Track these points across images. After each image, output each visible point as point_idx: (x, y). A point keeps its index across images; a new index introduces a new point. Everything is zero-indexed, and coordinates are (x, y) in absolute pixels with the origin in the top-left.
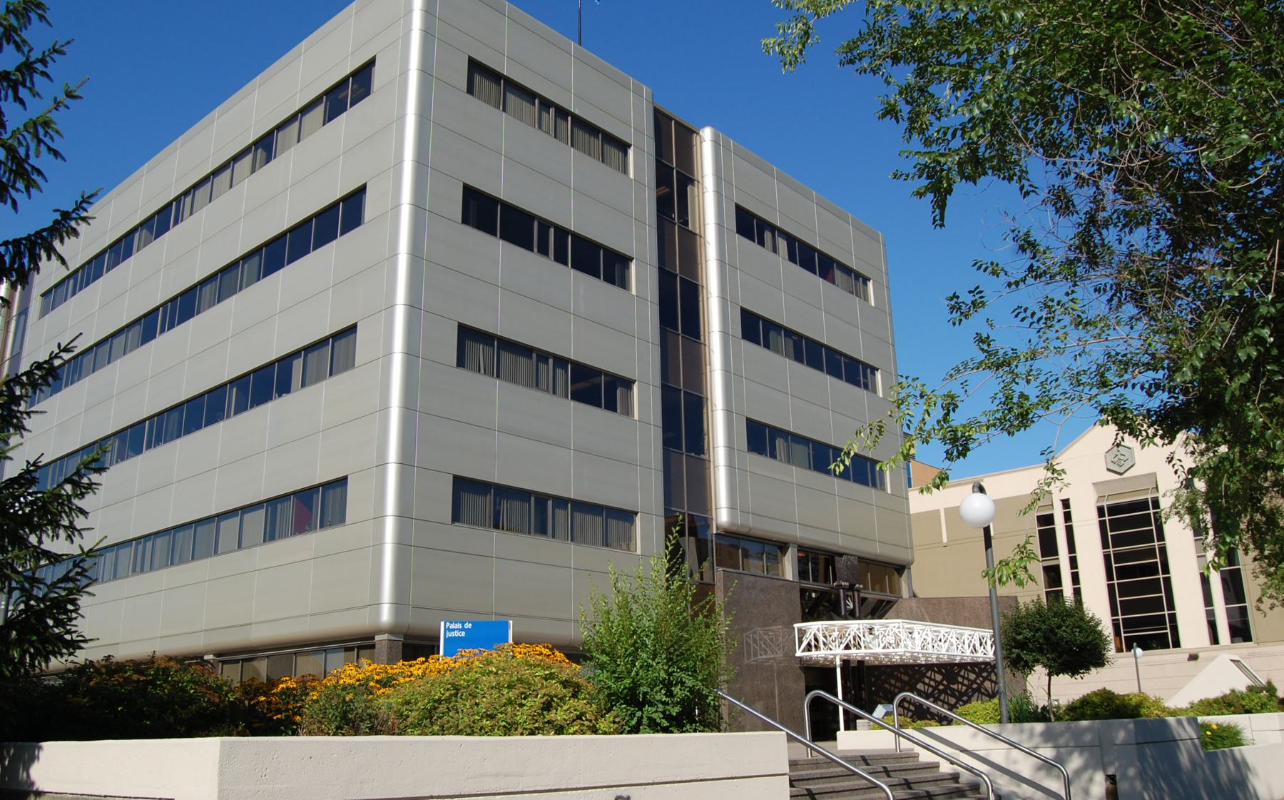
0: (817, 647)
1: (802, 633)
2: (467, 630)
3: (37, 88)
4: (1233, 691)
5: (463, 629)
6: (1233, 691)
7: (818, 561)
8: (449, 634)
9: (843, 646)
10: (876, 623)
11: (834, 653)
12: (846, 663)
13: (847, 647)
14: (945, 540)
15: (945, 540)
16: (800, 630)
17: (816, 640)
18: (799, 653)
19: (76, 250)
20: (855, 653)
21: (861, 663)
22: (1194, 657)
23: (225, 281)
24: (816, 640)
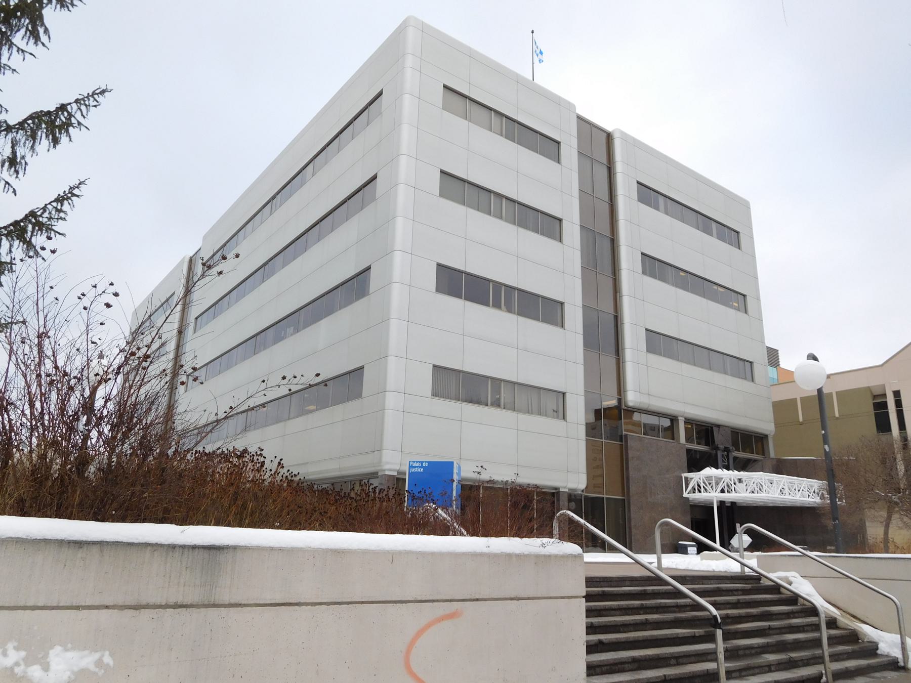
0: (728, 492)
1: (687, 481)
2: (424, 468)
3: (38, 148)
4: (73, 672)
5: (422, 467)
6: (73, 672)
7: (704, 431)
8: (412, 470)
9: (719, 490)
10: (742, 474)
11: (713, 496)
12: (722, 504)
13: (722, 491)
14: (801, 419)
15: (801, 419)
16: (686, 478)
17: (699, 486)
18: (685, 495)
19: (235, 271)
20: (728, 497)
21: (733, 503)
22: (202, 383)
23: (265, 269)
24: (699, 486)
